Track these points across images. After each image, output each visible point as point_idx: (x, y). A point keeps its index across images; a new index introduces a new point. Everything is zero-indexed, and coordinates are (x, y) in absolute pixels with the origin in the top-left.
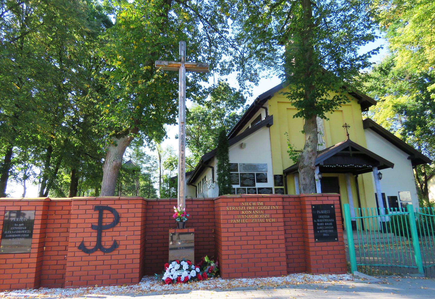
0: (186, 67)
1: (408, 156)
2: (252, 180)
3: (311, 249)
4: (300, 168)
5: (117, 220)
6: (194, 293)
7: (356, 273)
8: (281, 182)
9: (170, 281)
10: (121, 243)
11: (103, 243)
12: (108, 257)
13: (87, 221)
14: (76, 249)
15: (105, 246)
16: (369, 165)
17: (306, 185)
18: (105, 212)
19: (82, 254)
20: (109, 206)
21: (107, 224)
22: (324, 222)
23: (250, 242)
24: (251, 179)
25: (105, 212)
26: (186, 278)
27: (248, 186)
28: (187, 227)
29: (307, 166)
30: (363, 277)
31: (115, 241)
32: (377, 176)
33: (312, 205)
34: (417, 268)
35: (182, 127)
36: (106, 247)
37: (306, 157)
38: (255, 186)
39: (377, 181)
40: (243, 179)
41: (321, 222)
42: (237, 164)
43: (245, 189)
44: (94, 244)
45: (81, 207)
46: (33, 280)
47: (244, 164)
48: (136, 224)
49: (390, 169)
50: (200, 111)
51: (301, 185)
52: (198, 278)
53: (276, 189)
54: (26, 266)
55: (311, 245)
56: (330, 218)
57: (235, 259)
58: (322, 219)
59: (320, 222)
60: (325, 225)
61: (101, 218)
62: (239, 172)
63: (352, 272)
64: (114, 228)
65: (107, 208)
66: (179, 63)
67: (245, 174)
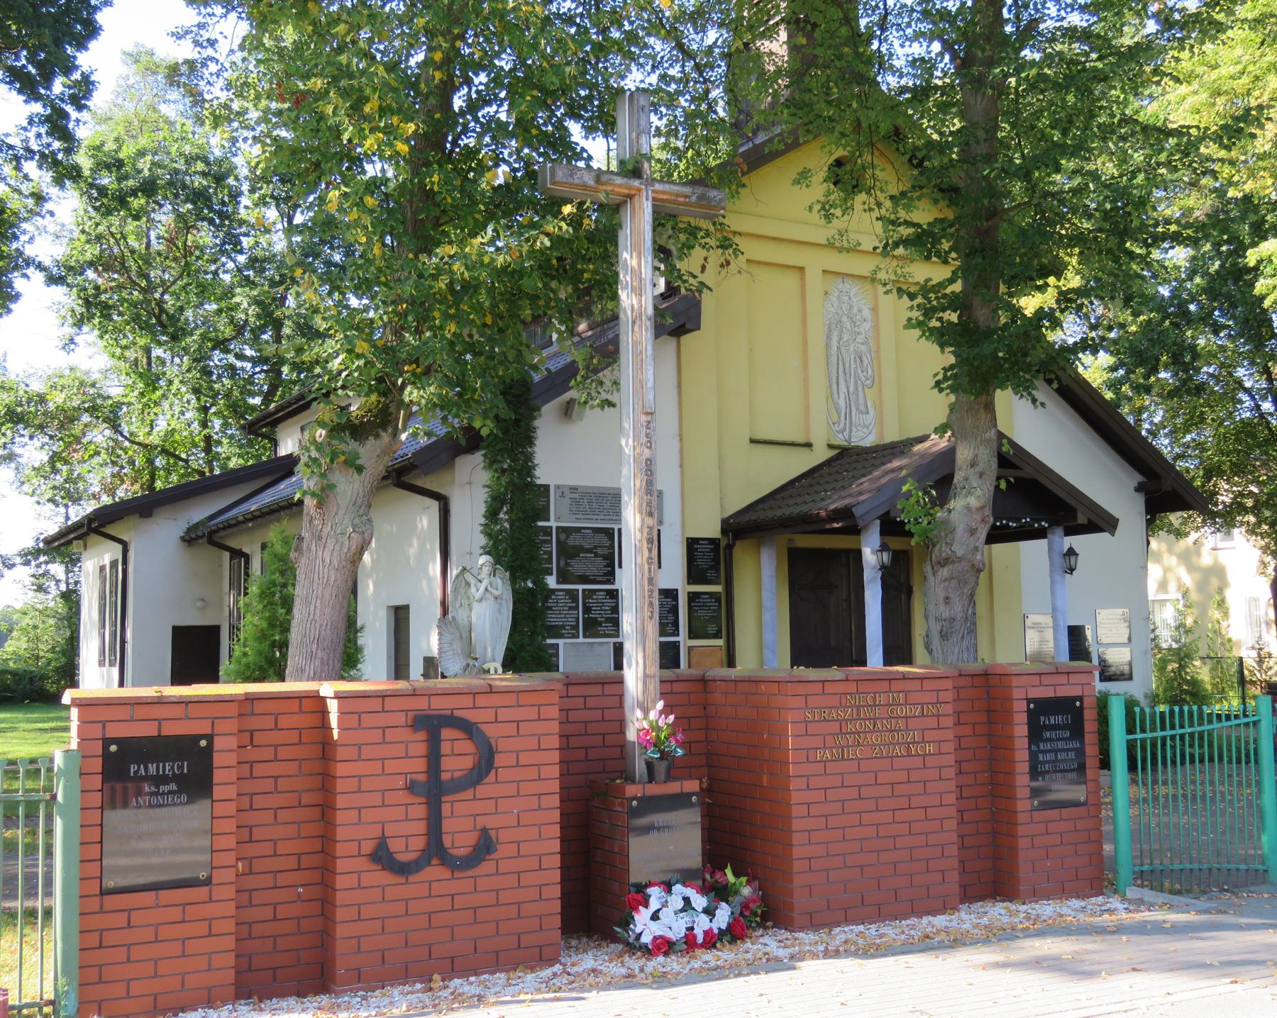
0: (654, 199)
1: (1138, 478)
2: (605, 557)
3: (1021, 830)
4: (939, 563)
5: (485, 763)
6: (809, 967)
7: (1132, 893)
8: (711, 568)
9: (664, 946)
10: (503, 835)
11: (447, 840)
12: (466, 885)
13: (391, 766)
14: (363, 863)
15: (453, 847)
16: (1039, 521)
17: (953, 619)
18: (446, 733)
19: (385, 878)
20: (456, 713)
21: (457, 774)
22: (1056, 751)
23: (866, 819)
24: (599, 551)
25: (446, 733)
26: (707, 933)
27: (584, 579)
28: (676, 779)
29: (960, 560)
30: (1160, 901)
31: (484, 831)
32: (1058, 560)
33: (1029, 701)
34: (1265, 871)
35: (648, 428)
36: (454, 852)
37: (960, 530)
38: (613, 583)
39: (1058, 578)
40: (567, 552)
41: (1049, 751)
42: (548, 486)
43: (573, 595)
44: (418, 843)
45: (367, 720)
46: (230, 976)
47: (574, 489)
48: (801, 783)
49: (1105, 535)
50: (187, 149)
51: (932, 621)
52: (734, 933)
53: (692, 597)
54: (202, 928)
55: (1022, 818)
56: (1071, 738)
57: (827, 870)
58: (1050, 740)
59: (1045, 752)
60: (1057, 760)
61: (434, 757)
62: (553, 523)
63: (1121, 887)
64: (478, 787)
65: (453, 721)
66: (636, 183)
67: (578, 530)
